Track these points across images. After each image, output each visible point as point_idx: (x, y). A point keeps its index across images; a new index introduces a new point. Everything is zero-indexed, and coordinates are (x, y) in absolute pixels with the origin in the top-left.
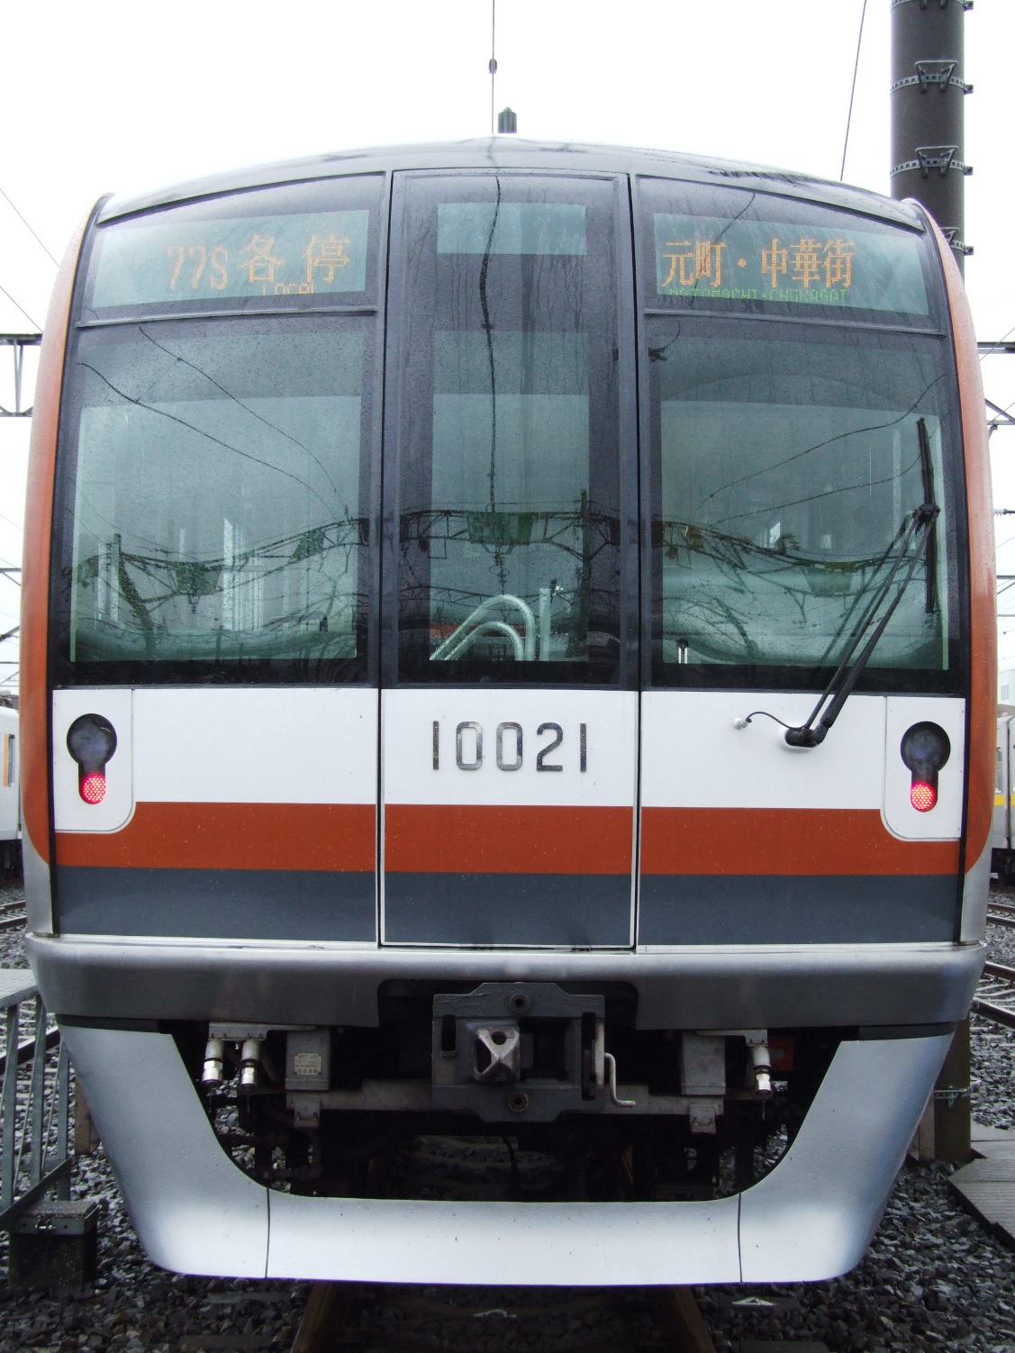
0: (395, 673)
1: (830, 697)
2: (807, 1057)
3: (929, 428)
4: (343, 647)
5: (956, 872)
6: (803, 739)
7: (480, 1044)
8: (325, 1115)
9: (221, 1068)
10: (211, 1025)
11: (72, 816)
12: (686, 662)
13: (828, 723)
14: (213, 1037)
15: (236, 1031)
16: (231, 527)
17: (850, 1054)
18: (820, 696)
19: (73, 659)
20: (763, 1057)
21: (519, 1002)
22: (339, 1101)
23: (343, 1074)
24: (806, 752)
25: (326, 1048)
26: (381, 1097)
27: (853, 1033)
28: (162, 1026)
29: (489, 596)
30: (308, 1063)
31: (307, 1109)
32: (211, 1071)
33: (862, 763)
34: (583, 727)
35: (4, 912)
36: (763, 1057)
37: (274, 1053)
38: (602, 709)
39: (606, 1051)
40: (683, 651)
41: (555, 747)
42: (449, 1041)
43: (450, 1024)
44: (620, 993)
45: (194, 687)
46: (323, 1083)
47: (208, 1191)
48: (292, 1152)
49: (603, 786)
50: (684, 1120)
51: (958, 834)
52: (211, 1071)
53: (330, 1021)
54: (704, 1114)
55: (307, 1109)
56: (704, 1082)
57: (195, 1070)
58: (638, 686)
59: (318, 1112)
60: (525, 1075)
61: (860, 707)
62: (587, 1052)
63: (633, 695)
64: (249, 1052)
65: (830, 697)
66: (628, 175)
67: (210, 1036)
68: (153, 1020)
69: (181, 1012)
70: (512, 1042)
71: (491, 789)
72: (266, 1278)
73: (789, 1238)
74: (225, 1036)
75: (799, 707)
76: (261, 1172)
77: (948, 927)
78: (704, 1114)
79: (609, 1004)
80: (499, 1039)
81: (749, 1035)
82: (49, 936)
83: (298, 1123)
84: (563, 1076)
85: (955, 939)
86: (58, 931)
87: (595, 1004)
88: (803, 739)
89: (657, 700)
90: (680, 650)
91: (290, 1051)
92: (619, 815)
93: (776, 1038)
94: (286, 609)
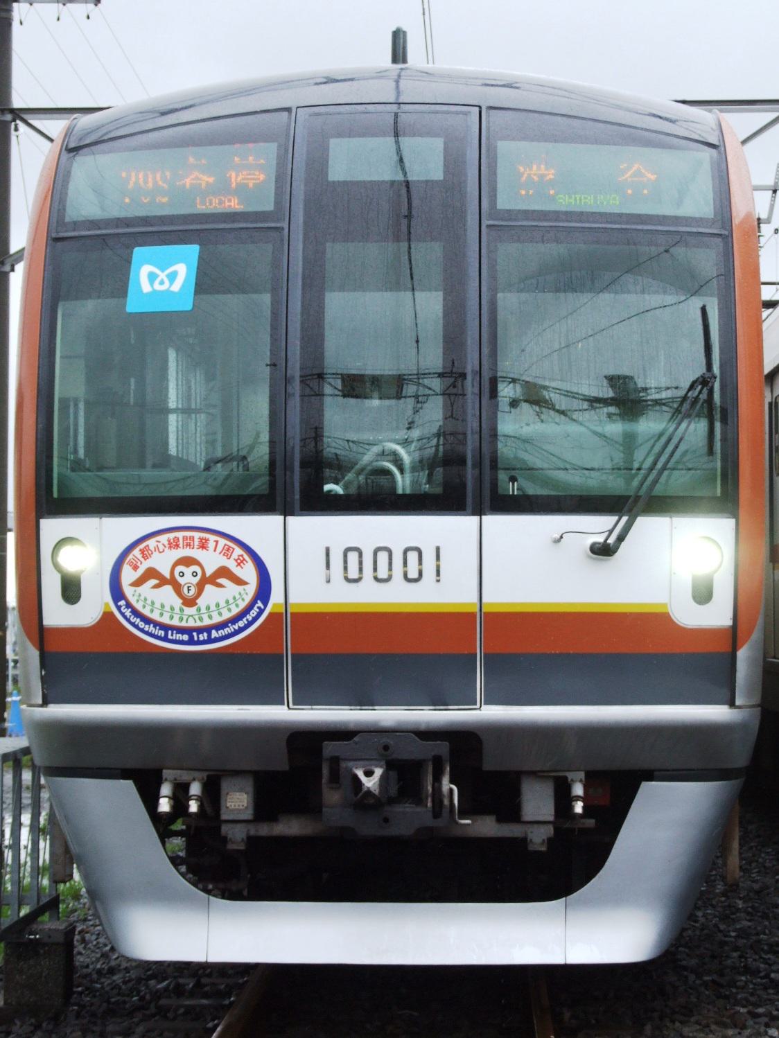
0: (297, 505)
1: (625, 519)
2: (616, 790)
3: (708, 309)
4: (260, 485)
5: (730, 650)
6: (603, 551)
7: (356, 778)
8: (251, 841)
9: (172, 804)
10: (164, 771)
11: (57, 614)
12: (516, 493)
13: (621, 538)
14: (166, 780)
15: (184, 776)
16: (175, 355)
17: (649, 791)
18: (617, 518)
19: (55, 495)
20: (578, 790)
21: (386, 748)
22: (264, 830)
23: (265, 809)
24: (609, 559)
25: (250, 789)
26: (290, 827)
27: (650, 776)
28: (125, 774)
29: (375, 445)
30: (237, 801)
31: (236, 835)
32: (164, 806)
34: (438, 549)
36: (578, 790)
38: (447, 532)
39: (452, 782)
40: (513, 485)
42: (335, 777)
43: (335, 761)
44: (464, 744)
45: (150, 516)
46: (248, 815)
47: (157, 895)
48: (223, 868)
49: (450, 592)
50: (523, 841)
51: (729, 623)
52: (164, 806)
53: (256, 768)
54: (539, 837)
55: (236, 835)
56: (537, 804)
57: (150, 800)
58: (479, 511)
59: (245, 838)
60: (392, 801)
61: (649, 527)
62: (436, 784)
63: (476, 519)
64: (195, 789)
65: (625, 519)
66: (480, 107)
67: (164, 779)
68: (117, 769)
69: (139, 762)
70: (378, 772)
71: (369, 596)
72: (206, 962)
73: (604, 930)
74: (175, 779)
75: (598, 526)
77: (725, 692)
78: (539, 837)
79: (454, 753)
80: (369, 774)
81: (570, 775)
82: (42, 706)
83: (230, 846)
84: (419, 800)
85: (732, 704)
86: (45, 703)
87: (443, 748)
88: (603, 551)
89: (493, 522)
90: (511, 483)
91: (223, 792)
93: (591, 779)
94: (219, 453)
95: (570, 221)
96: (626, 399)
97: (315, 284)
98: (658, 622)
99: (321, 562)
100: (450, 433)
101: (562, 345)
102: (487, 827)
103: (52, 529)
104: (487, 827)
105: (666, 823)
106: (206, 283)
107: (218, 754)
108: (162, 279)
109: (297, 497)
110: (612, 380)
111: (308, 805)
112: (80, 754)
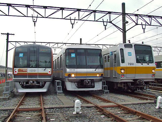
2: (45, 82)
11: (15, 73)
23: (26, 84)
27: (47, 82)
30: (25, 83)
32: (21, 84)
33: (48, 71)
35: (161, 93)
37: (23, 83)
41: (124, 58)
47: (20, 89)
48: (23, 87)
49: (36, 72)
56: (41, 83)
57: (20, 84)
71: (32, 72)
75: (44, 69)
76: (22, 88)
88: (44, 70)
92: (37, 73)
93: (44, 82)
95: (10, 115)
96: (46, 62)
97: (29, 56)
98: (47, 74)
99: (29, 70)
100: (36, 64)
101: (42, 59)
102: (38, 85)
103: (15, 69)
104: (38, 85)
105: (47, 84)
106: (23, 55)
107: (24, 81)
108: (21, 55)
109: (26, 78)
110: (45, 61)
111: (28, 83)
112: (16, 81)
